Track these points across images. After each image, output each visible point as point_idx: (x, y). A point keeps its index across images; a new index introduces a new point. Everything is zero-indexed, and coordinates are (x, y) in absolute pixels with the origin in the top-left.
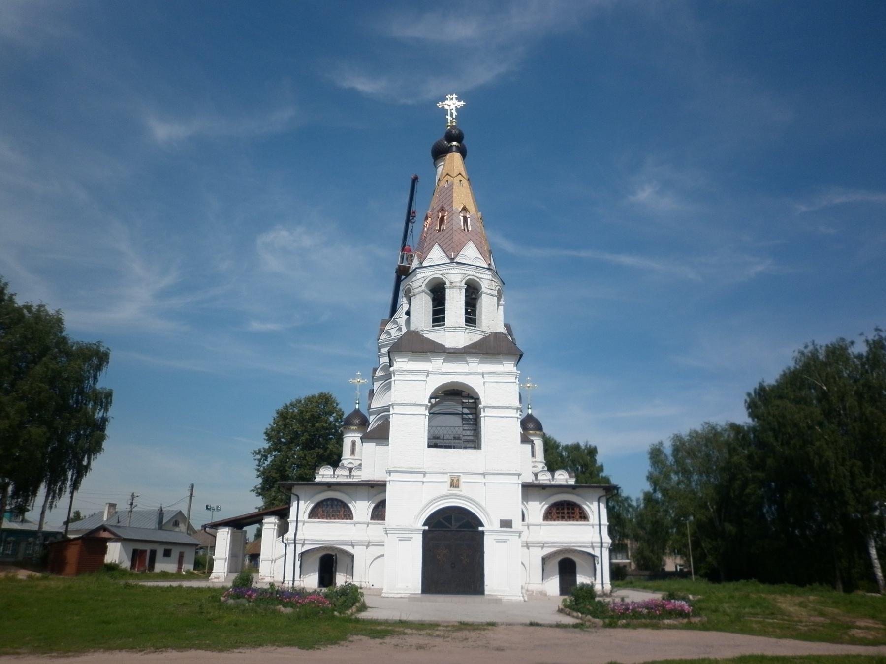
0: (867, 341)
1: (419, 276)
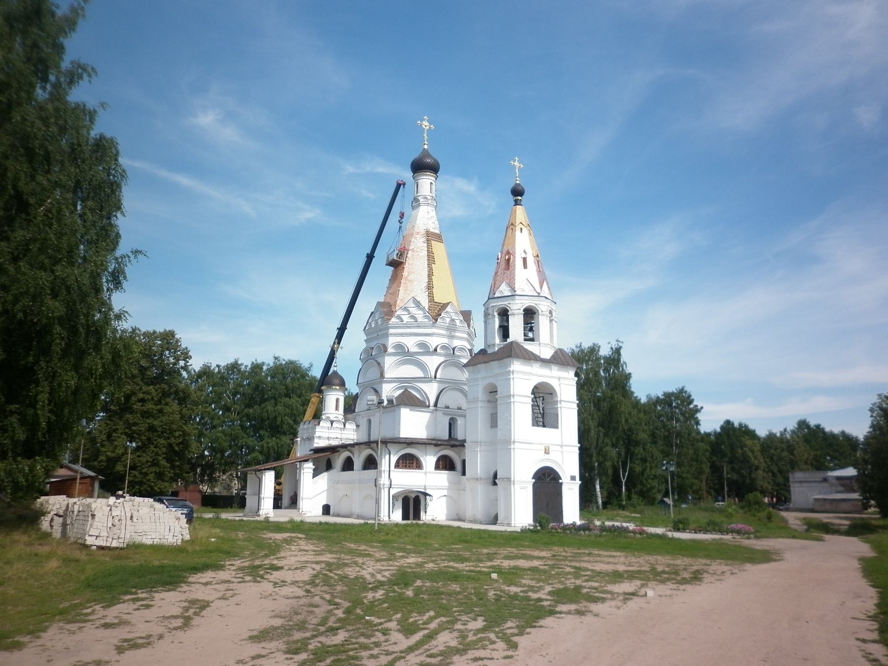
0: (612, 348)
1: (517, 302)
